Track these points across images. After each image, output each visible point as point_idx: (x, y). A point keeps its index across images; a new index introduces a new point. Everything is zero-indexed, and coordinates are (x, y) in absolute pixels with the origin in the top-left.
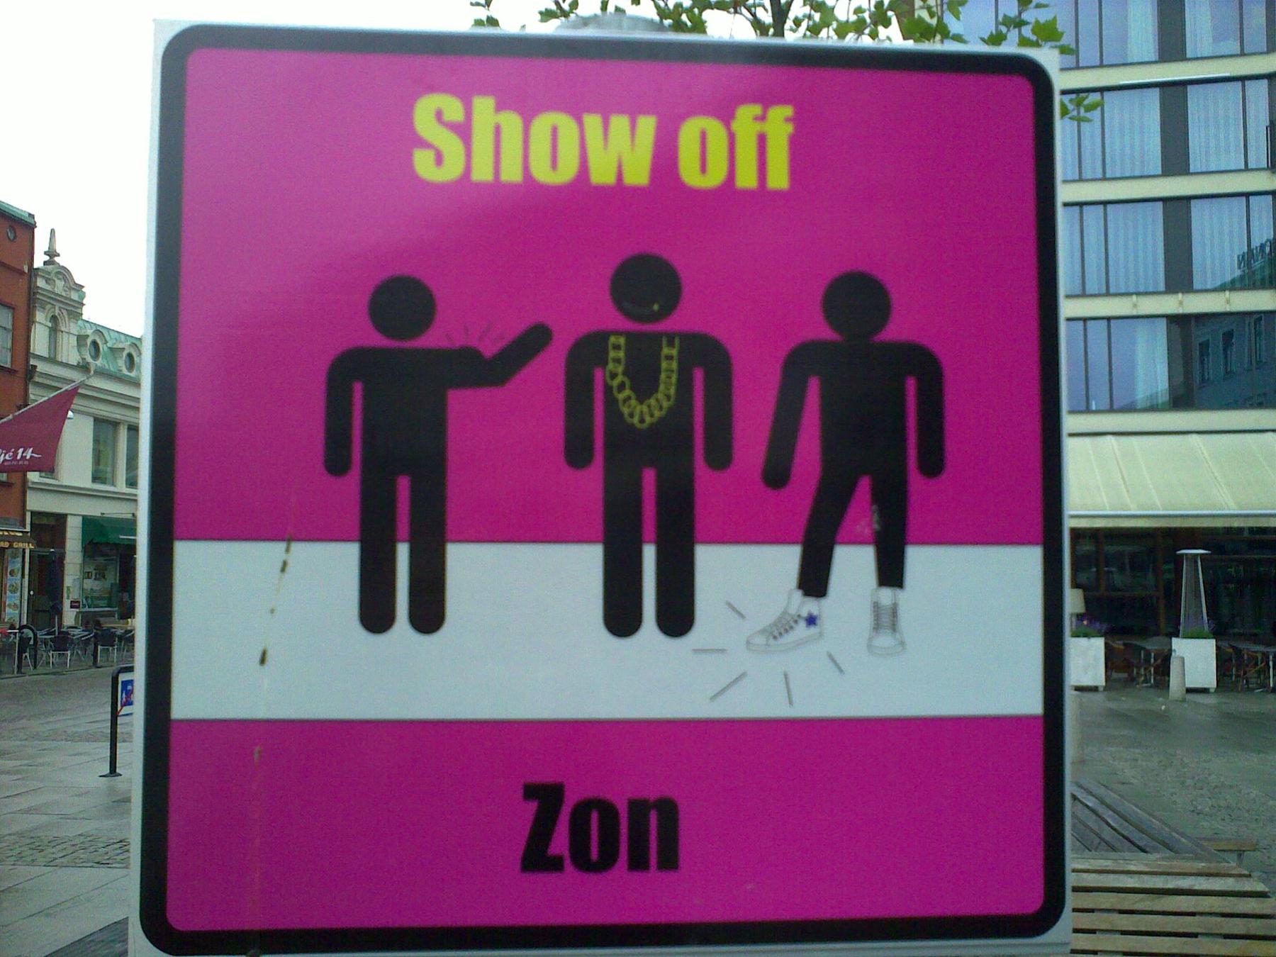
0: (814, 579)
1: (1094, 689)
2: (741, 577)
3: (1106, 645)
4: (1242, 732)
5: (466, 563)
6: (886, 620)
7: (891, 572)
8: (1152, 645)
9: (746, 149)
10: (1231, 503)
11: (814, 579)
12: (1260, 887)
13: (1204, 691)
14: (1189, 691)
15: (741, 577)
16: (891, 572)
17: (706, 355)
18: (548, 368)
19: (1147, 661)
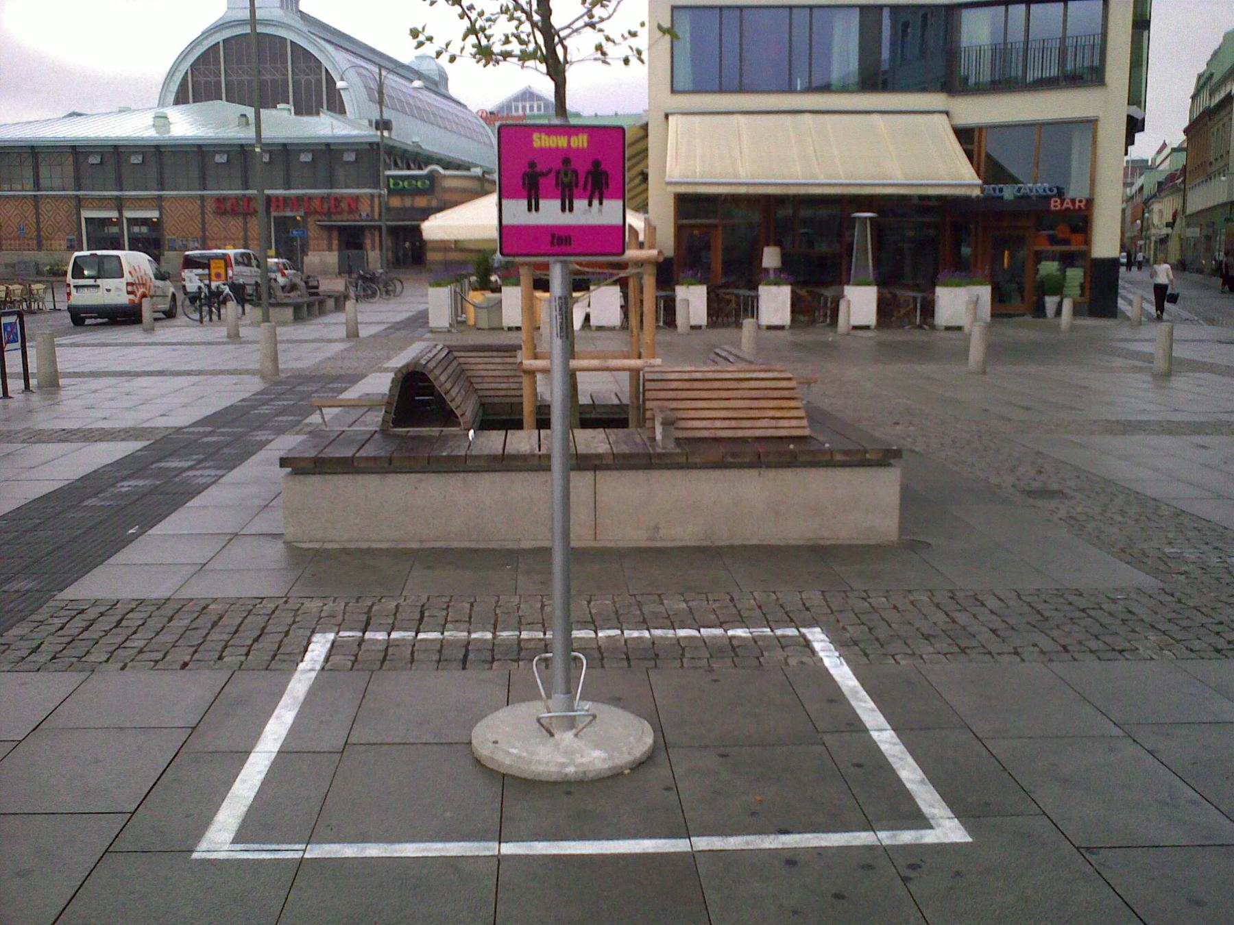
0: (590, 204)
1: (782, 328)
2: (580, 204)
3: (792, 292)
4: (887, 352)
5: (542, 203)
6: (600, 211)
7: (601, 203)
8: (829, 293)
9: (580, 141)
10: (898, 173)
11: (590, 204)
12: (790, 375)
13: (867, 328)
14: (855, 328)
15: (580, 204)
16: (601, 203)
17: (575, 172)
18: (553, 174)
19: (826, 304)
